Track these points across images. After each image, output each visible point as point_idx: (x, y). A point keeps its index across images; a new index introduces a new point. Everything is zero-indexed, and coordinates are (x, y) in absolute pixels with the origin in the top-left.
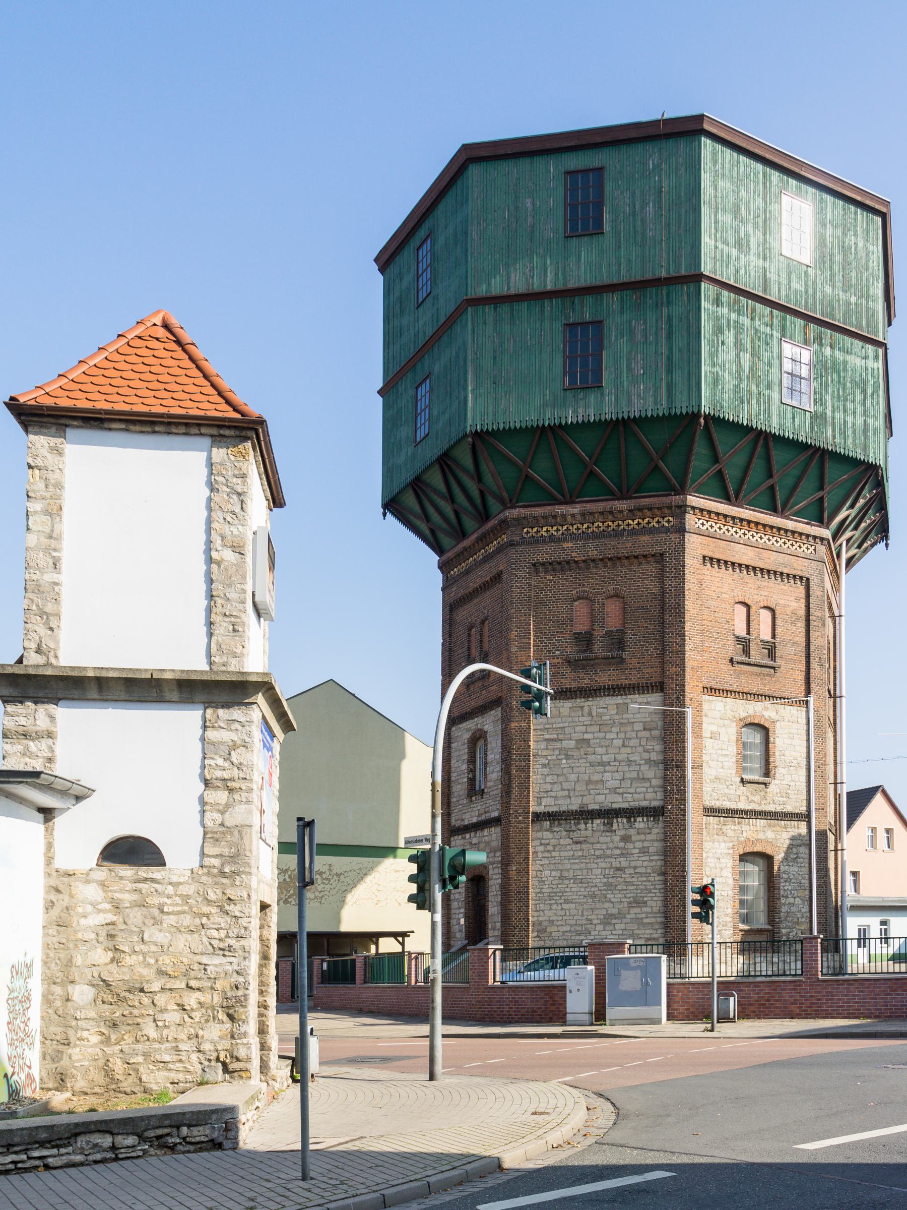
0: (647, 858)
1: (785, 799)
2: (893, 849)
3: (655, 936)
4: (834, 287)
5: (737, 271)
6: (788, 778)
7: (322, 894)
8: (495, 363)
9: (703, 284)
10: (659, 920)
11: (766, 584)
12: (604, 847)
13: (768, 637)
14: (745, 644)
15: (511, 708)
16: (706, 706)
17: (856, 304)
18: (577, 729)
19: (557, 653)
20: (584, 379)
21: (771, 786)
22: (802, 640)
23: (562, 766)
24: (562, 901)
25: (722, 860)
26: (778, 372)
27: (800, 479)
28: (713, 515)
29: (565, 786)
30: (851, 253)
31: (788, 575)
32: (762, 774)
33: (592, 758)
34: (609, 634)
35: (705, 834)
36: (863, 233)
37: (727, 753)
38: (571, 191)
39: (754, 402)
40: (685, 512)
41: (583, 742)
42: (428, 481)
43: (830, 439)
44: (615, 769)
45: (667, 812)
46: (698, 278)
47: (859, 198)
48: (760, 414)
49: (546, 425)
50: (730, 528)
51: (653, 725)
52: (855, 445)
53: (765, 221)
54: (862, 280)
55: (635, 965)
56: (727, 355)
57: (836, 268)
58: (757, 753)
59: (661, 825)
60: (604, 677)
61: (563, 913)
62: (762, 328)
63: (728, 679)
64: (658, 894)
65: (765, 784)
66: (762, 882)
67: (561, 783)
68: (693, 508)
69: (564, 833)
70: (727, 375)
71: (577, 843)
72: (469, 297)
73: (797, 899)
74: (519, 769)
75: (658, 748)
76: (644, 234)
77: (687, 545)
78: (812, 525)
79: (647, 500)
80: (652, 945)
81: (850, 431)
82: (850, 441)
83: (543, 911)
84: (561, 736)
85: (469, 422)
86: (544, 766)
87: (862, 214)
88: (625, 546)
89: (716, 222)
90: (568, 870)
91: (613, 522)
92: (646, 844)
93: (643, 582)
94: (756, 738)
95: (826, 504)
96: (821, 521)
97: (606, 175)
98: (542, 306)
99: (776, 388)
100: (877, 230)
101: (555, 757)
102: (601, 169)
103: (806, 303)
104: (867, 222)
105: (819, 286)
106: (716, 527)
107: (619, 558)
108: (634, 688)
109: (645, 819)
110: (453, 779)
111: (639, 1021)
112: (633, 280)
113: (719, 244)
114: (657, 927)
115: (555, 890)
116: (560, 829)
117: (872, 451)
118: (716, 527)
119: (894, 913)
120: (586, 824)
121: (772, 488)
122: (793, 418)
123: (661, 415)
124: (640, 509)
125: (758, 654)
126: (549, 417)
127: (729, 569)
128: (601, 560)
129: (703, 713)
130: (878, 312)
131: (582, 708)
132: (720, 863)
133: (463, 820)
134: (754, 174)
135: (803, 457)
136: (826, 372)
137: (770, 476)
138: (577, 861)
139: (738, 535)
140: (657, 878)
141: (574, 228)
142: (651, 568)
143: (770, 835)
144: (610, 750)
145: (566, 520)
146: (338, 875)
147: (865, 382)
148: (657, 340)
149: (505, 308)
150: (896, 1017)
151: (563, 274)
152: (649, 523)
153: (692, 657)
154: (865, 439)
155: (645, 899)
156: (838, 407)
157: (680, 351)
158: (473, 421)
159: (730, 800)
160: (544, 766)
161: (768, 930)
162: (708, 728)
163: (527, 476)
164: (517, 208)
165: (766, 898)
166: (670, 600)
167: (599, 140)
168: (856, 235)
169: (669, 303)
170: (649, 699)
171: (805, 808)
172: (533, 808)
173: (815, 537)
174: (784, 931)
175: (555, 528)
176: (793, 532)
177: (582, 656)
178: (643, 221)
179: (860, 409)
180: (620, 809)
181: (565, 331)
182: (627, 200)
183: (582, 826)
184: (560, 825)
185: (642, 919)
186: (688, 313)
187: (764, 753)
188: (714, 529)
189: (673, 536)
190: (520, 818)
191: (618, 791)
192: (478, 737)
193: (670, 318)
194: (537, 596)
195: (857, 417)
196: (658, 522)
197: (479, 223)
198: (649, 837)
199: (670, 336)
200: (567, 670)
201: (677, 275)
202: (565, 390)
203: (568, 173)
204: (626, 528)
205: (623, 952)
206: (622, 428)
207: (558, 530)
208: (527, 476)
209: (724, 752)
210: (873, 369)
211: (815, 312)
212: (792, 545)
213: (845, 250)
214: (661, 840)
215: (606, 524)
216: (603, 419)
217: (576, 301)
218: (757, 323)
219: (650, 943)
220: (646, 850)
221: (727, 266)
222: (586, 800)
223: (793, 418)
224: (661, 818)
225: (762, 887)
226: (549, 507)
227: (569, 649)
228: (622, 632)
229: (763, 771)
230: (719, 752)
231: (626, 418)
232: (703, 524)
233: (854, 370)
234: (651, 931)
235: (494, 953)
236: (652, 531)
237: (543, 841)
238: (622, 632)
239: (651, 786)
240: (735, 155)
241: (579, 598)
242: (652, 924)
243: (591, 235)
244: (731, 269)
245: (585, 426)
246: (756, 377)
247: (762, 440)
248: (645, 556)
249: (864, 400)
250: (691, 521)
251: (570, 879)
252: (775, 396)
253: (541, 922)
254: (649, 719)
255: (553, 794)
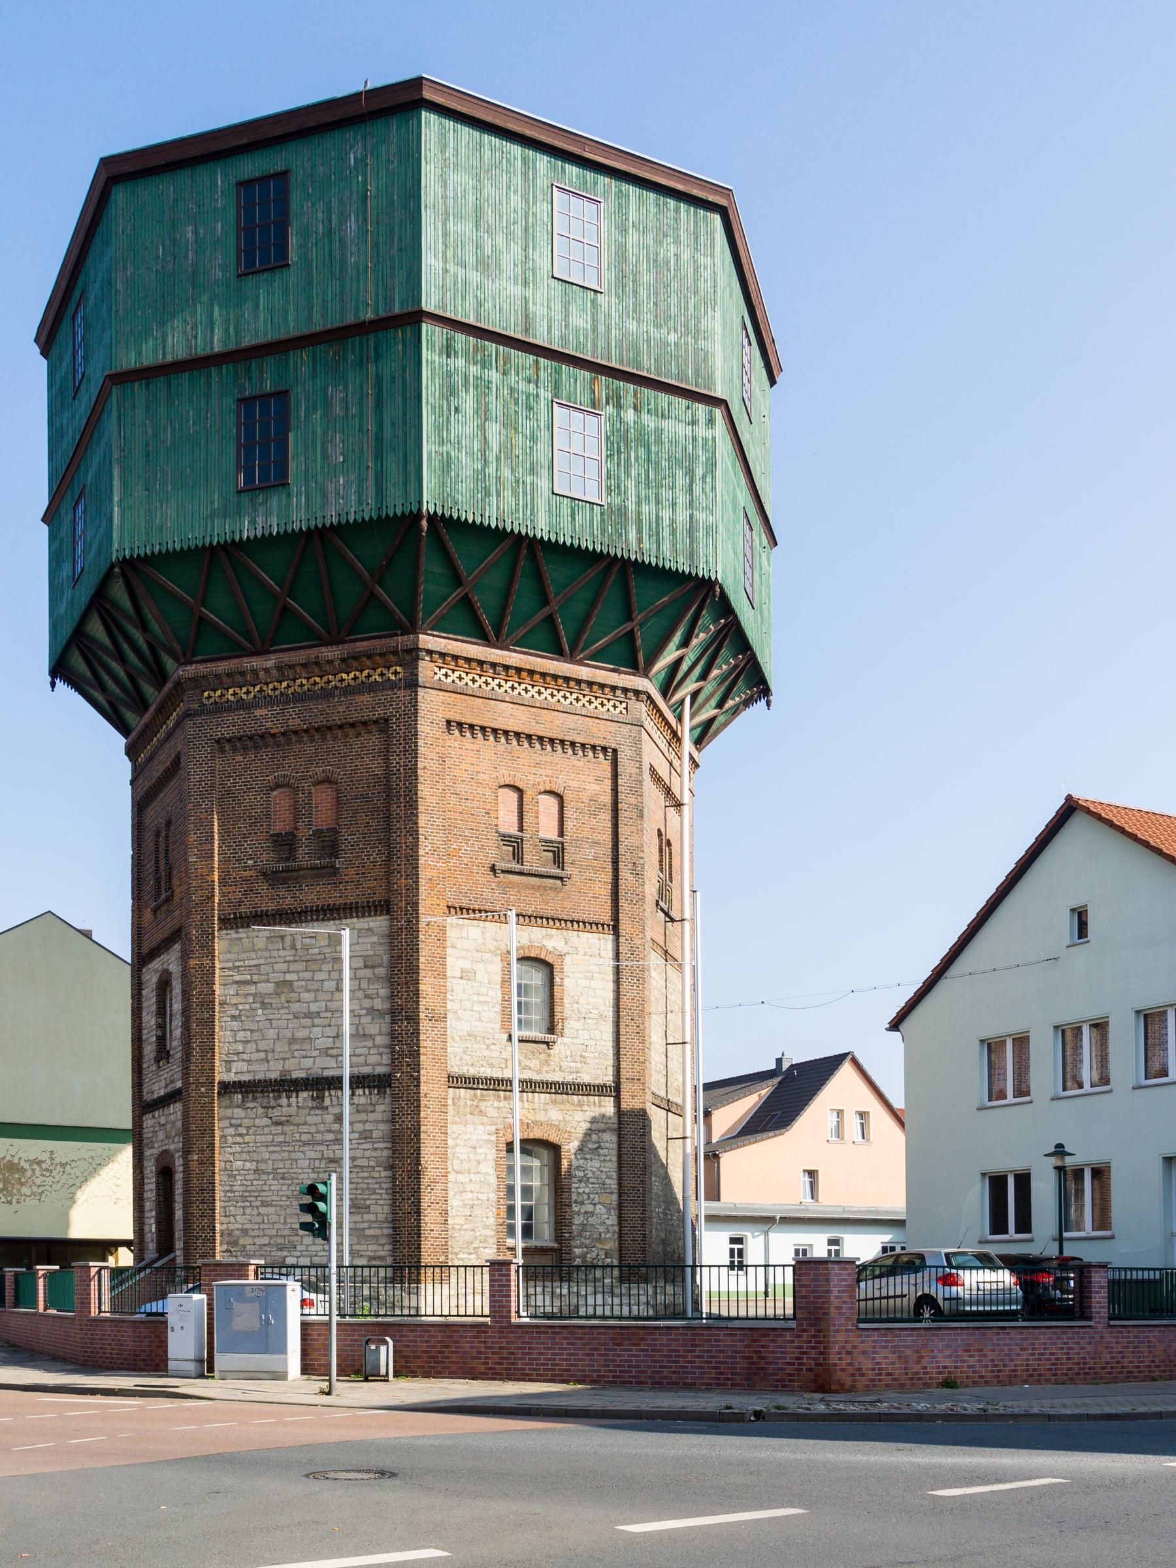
0: (370, 1146)
1: (579, 1065)
2: (868, 1140)
3: (381, 1253)
4: (639, 321)
5: (480, 305)
6: (586, 1035)
7: (42, 1189)
8: (147, 462)
9: (424, 325)
10: (386, 1232)
11: (548, 759)
12: (313, 1129)
13: (553, 835)
14: (516, 845)
15: (190, 940)
16: (451, 934)
17: (676, 344)
18: (276, 967)
19: (250, 862)
20: (264, 476)
21: (556, 1047)
22: (607, 838)
23: (257, 1018)
24: (258, 1203)
25: (478, 1150)
26: (548, 449)
27: (593, 605)
28: (461, 662)
29: (262, 1045)
30: (669, 270)
31: (583, 745)
32: (544, 1029)
33: (296, 1007)
34: (318, 834)
35: (451, 1110)
36: (698, 243)
37: (487, 999)
38: (245, 208)
39: (507, 493)
40: (417, 658)
41: (284, 985)
42: (92, 633)
43: (633, 544)
44: (327, 1022)
45: (394, 1082)
46: (416, 317)
47: (680, 187)
48: (517, 511)
49: (215, 543)
50: (490, 680)
51: (377, 961)
52: (674, 550)
53: (526, 230)
54: (687, 309)
55: (253, 1295)
56: (465, 427)
57: (643, 293)
58: (537, 999)
59: (388, 1100)
60: (313, 894)
61: (259, 1219)
62: (522, 386)
63: (488, 894)
64: (384, 1196)
65: (547, 1043)
66: (546, 1181)
67: (256, 1041)
68: (430, 652)
69: (261, 1111)
70: (463, 456)
71: (277, 1124)
72: (113, 371)
73: (598, 1207)
74: (201, 1022)
75: (384, 992)
76: (343, 261)
77: (421, 706)
78: (620, 672)
79: (364, 643)
80: (378, 1267)
81: (667, 531)
82: (666, 546)
83: (234, 1216)
84: (255, 978)
85: (116, 546)
86: (234, 1018)
87: (688, 211)
88: (337, 711)
89: (445, 234)
90: (265, 1161)
91: (321, 677)
92: (368, 1127)
93: (361, 759)
94: (537, 978)
95: (639, 642)
96: (634, 663)
97: (292, 180)
98: (209, 376)
99: (545, 472)
100: (713, 232)
101: (247, 1007)
102: (284, 175)
103: (595, 346)
104: (696, 223)
105: (615, 319)
106: (466, 679)
107: (329, 728)
108: (351, 908)
109: (367, 1091)
110: (144, 1037)
111: (261, 1375)
112: (329, 326)
113: (451, 267)
114: (383, 1241)
115: (250, 1188)
116: (255, 1107)
117: (703, 560)
118: (467, 679)
119: (850, 1228)
120: (289, 1098)
121: (550, 619)
122: (573, 515)
123: (367, 519)
124: (356, 658)
125: (534, 859)
126: (220, 531)
127: (485, 741)
128: (306, 731)
129: (448, 943)
130: (713, 355)
131: (283, 937)
132: (475, 1154)
133: (152, 1093)
134: (508, 161)
135: (594, 572)
136: (626, 445)
137: (546, 602)
138: (278, 1149)
139: (503, 689)
140: (384, 1174)
141: (250, 263)
142: (373, 740)
143: (555, 1115)
144: (321, 996)
145: (258, 677)
146: (63, 1165)
147: (692, 459)
148: (361, 414)
149: (160, 383)
150: (621, 1382)
151: (236, 328)
152: (369, 676)
153: (429, 863)
154: (692, 542)
155: (368, 1202)
156: (647, 498)
157: (393, 424)
158: (120, 544)
159: (491, 1066)
160: (234, 1018)
161: (552, 1249)
162: (454, 964)
163: (200, 618)
164: (174, 242)
165: (552, 1204)
166: (400, 785)
167: (279, 131)
168: (677, 242)
169: (378, 358)
170: (372, 924)
171: (611, 1078)
172: (221, 1075)
173: (625, 690)
174: (577, 1251)
175: (244, 690)
176: (590, 684)
177: (281, 866)
178: (342, 243)
179: (682, 499)
180: (333, 1078)
181: (239, 409)
182: (320, 215)
183: (284, 1101)
184: (254, 1099)
185: (363, 1230)
186: (404, 370)
187: (547, 1000)
188: (463, 682)
189: (401, 693)
190: (203, 1089)
191: (331, 1052)
192: (164, 984)
193: (379, 380)
194: (223, 785)
195: (679, 510)
196: (382, 675)
197: (125, 268)
198: (372, 1117)
199: (379, 405)
200: (262, 886)
201: (389, 315)
202: (239, 492)
203: (240, 184)
204: (339, 684)
205: (246, 1277)
206: (318, 540)
207: (248, 692)
208: (200, 618)
209: (482, 999)
210: (705, 440)
211: (609, 359)
212: (590, 702)
213: (658, 265)
214: (388, 1121)
215: (312, 680)
216: (289, 530)
217: (254, 366)
218: (513, 378)
219: (374, 1263)
220: (368, 1135)
221: (464, 298)
222: (290, 1065)
223: (573, 515)
224: (388, 1090)
225: (546, 1188)
226: (235, 661)
227: (265, 857)
228: (335, 831)
229: (545, 1025)
230: (475, 998)
231: (320, 526)
232: (446, 675)
233: (673, 442)
234: (375, 1247)
235: (99, 1272)
236: (373, 688)
237: (233, 1121)
238: (335, 831)
239: (374, 1046)
240: (476, 134)
241: (278, 786)
242: (376, 1237)
243: (274, 268)
244: (470, 303)
245: (266, 542)
246: (512, 459)
247: (526, 553)
248: (364, 724)
249: (691, 485)
250: (426, 670)
251: (269, 1174)
252: (543, 484)
253: (232, 1230)
254: (371, 953)
255: (245, 1056)
